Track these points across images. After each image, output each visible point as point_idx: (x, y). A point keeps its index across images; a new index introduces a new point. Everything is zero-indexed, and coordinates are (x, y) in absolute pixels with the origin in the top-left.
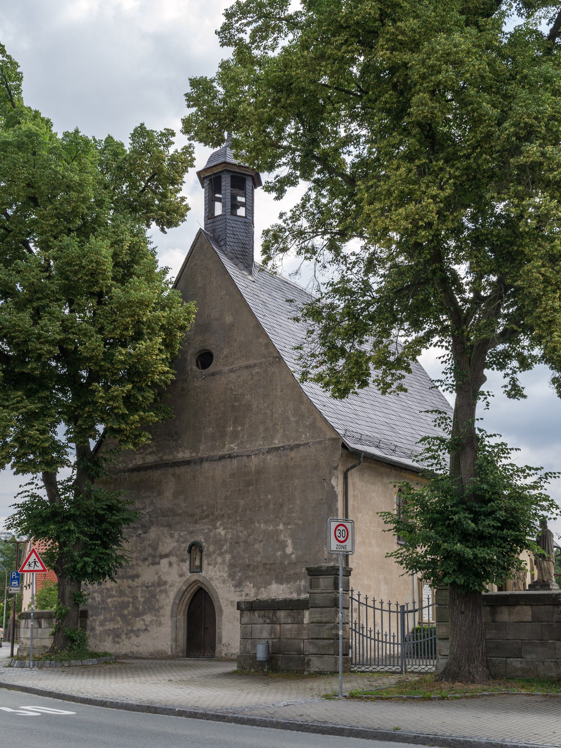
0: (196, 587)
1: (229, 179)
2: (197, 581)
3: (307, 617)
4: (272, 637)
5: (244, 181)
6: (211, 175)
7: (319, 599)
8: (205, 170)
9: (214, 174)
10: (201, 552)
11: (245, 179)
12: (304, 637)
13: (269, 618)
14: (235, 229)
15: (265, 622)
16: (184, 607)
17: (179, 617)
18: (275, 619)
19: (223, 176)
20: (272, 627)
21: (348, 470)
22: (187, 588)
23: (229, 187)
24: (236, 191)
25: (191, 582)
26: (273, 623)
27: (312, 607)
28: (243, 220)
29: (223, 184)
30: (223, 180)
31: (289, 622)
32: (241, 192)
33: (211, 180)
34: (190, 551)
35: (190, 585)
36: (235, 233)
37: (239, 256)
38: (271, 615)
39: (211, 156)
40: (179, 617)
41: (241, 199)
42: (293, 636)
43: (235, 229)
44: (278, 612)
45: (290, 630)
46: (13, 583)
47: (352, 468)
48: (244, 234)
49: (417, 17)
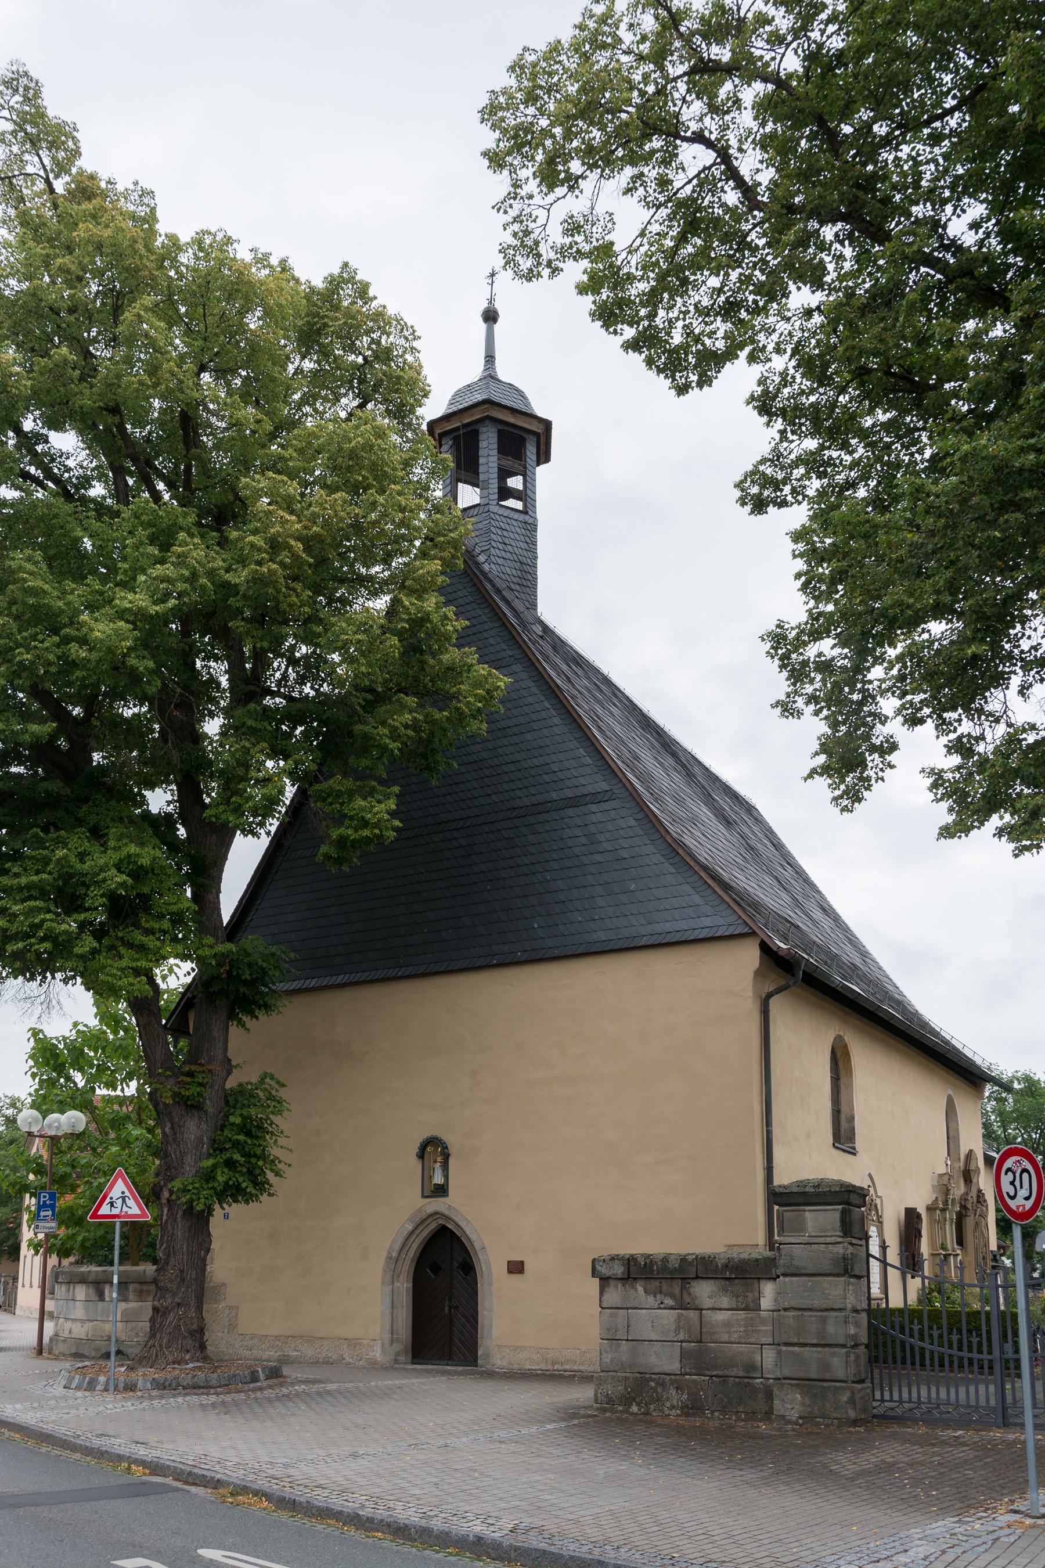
0: (434, 1225)
1: (495, 440)
2: (436, 1213)
3: (768, 1294)
4: (681, 1337)
5: (523, 441)
6: (457, 429)
7: (797, 1253)
8: (446, 418)
9: (465, 426)
10: (446, 1157)
11: (524, 440)
12: (764, 1340)
13: (672, 1296)
14: (505, 533)
15: (661, 1306)
16: (407, 1267)
17: (397, 1284)
18: (687, 1299)
19: (483, 429)
20: (680, 1316)
21: (769, 996)
22: (416, 1228)
23: (495, 452)
24: (509, 463)
25: (424, 1215)
26: (682, 1306)
27: (785, 1275)
28: (522, 517)
29: (483, 444)
30: (482, 437)
31: (725, 1305)
32: (517, 465)
33: (456, 440)
34: (421, 1155)
35: (423, 1221)
36: (507, 541)
37: (513, 586)
38: (677, 1290)
39: (456, 394)
40: (397, 1284)
41: (515, 482)
42: (735, 1337)
43: (505, 533)
44: (694, 1283)
45: (727, 1324)
46: (42, 1214)
47: (778, 991)
48: (523, 545)
49: (81, 957)
